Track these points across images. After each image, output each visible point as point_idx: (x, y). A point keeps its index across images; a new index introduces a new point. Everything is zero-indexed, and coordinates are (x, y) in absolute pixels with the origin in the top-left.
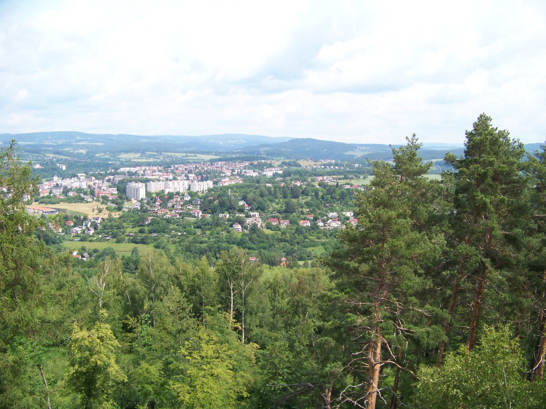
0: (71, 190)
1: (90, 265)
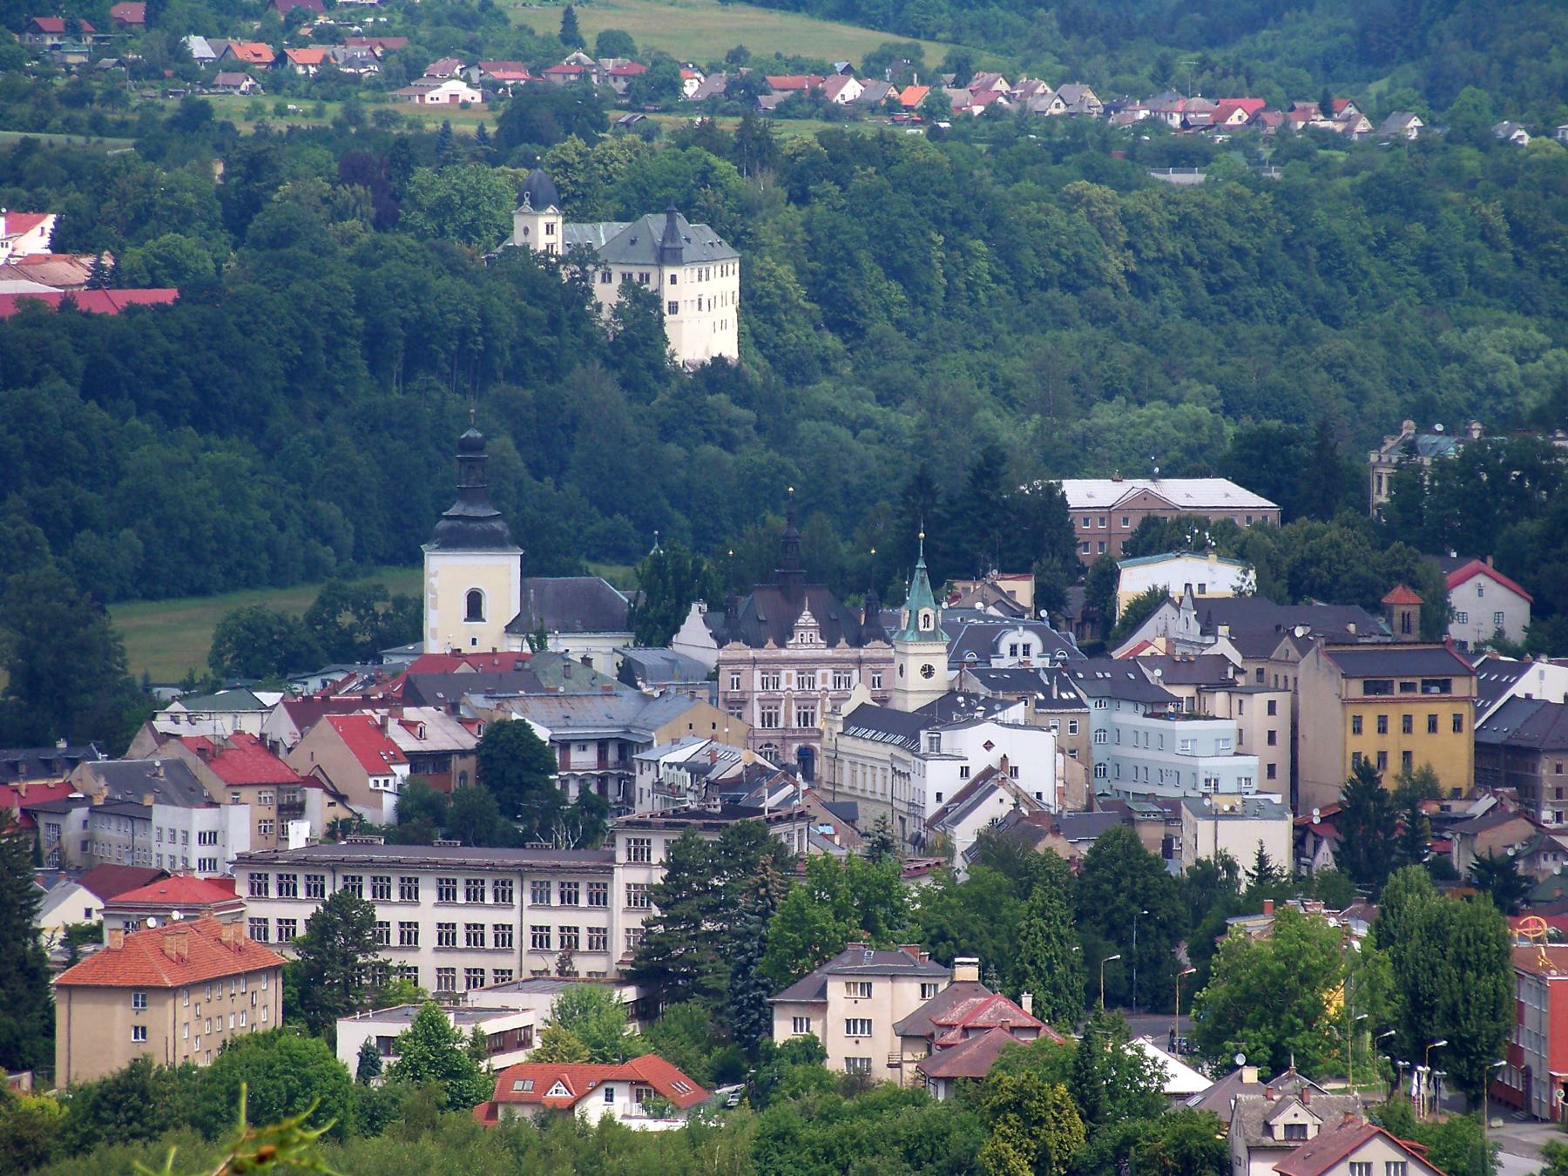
0: (867, 913)
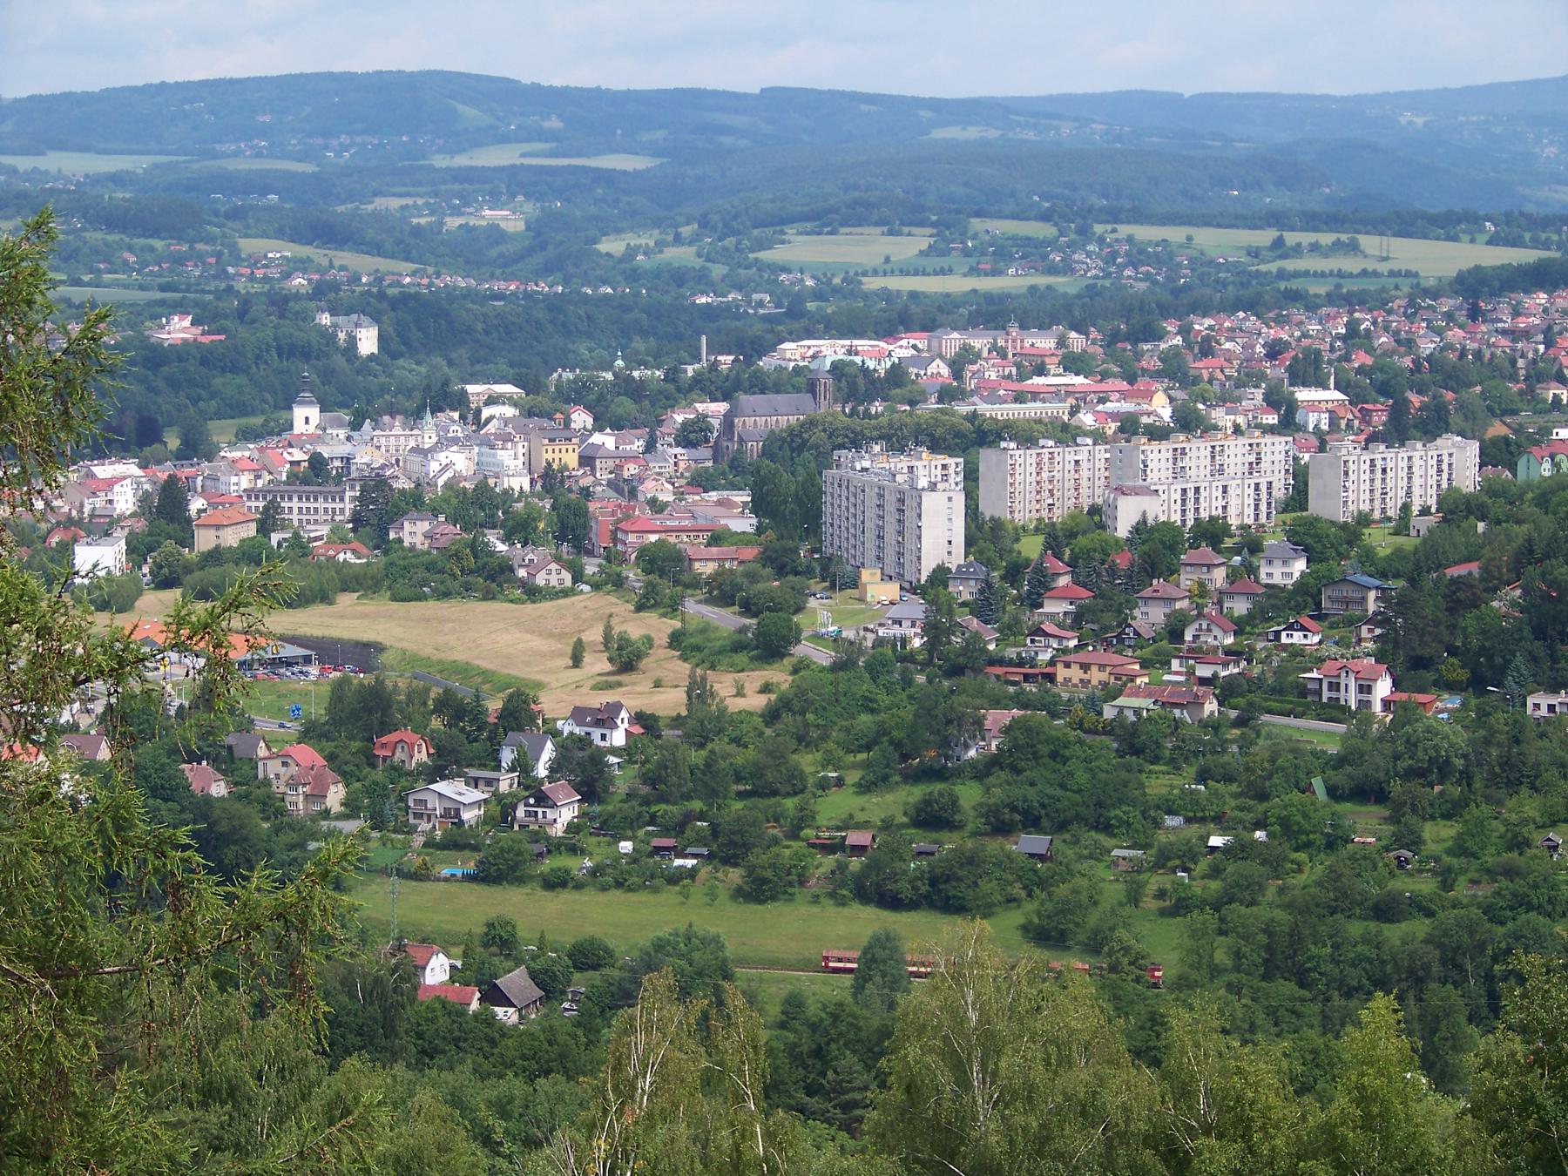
1: (544, 1058)
